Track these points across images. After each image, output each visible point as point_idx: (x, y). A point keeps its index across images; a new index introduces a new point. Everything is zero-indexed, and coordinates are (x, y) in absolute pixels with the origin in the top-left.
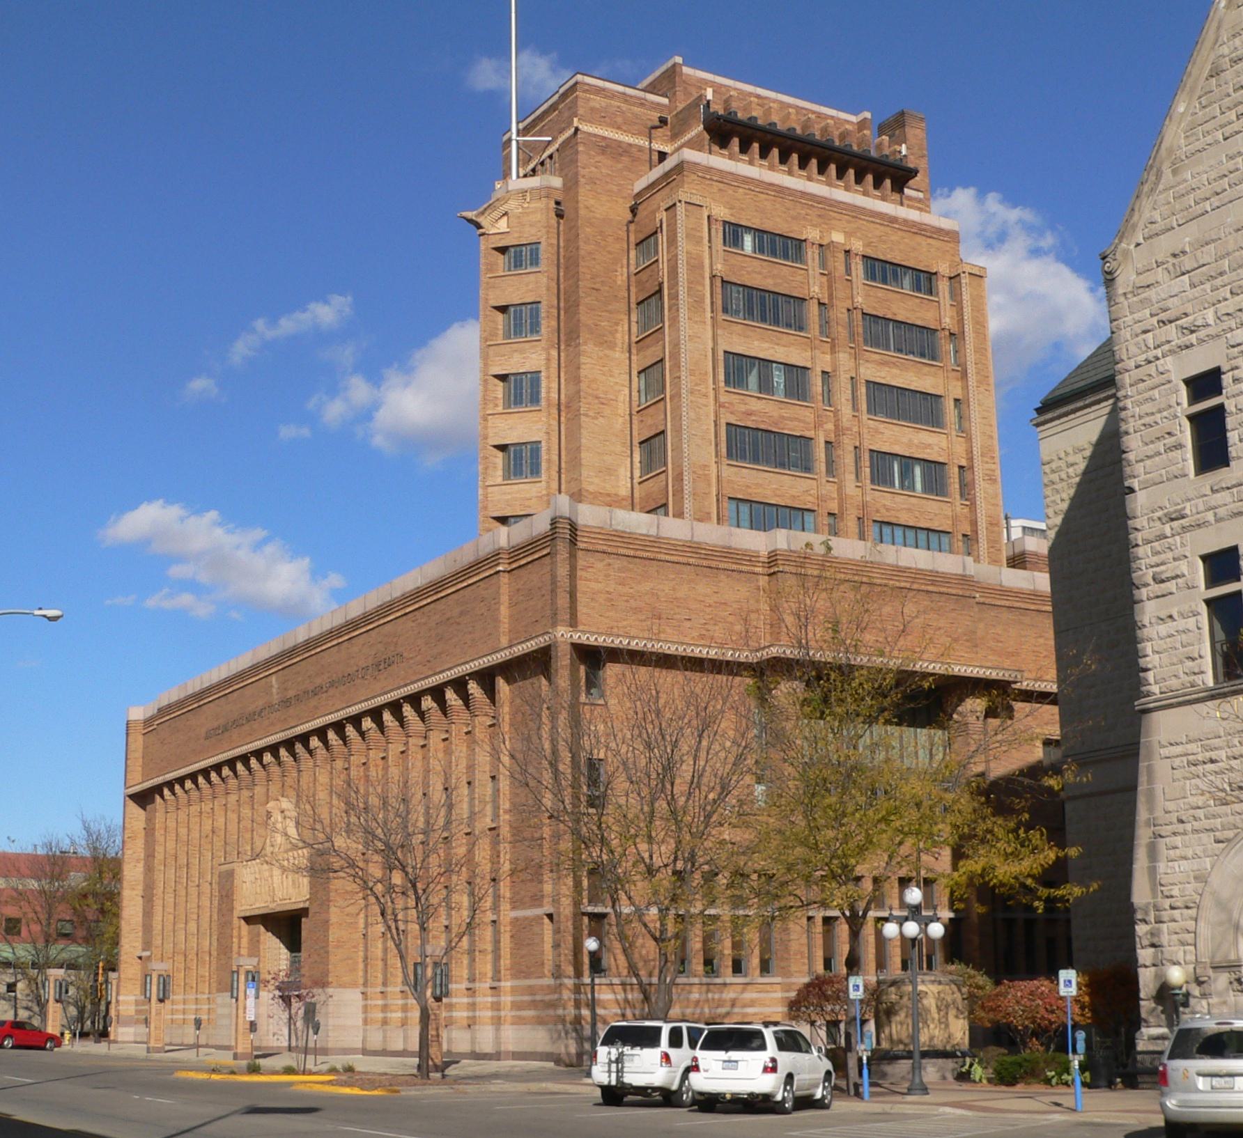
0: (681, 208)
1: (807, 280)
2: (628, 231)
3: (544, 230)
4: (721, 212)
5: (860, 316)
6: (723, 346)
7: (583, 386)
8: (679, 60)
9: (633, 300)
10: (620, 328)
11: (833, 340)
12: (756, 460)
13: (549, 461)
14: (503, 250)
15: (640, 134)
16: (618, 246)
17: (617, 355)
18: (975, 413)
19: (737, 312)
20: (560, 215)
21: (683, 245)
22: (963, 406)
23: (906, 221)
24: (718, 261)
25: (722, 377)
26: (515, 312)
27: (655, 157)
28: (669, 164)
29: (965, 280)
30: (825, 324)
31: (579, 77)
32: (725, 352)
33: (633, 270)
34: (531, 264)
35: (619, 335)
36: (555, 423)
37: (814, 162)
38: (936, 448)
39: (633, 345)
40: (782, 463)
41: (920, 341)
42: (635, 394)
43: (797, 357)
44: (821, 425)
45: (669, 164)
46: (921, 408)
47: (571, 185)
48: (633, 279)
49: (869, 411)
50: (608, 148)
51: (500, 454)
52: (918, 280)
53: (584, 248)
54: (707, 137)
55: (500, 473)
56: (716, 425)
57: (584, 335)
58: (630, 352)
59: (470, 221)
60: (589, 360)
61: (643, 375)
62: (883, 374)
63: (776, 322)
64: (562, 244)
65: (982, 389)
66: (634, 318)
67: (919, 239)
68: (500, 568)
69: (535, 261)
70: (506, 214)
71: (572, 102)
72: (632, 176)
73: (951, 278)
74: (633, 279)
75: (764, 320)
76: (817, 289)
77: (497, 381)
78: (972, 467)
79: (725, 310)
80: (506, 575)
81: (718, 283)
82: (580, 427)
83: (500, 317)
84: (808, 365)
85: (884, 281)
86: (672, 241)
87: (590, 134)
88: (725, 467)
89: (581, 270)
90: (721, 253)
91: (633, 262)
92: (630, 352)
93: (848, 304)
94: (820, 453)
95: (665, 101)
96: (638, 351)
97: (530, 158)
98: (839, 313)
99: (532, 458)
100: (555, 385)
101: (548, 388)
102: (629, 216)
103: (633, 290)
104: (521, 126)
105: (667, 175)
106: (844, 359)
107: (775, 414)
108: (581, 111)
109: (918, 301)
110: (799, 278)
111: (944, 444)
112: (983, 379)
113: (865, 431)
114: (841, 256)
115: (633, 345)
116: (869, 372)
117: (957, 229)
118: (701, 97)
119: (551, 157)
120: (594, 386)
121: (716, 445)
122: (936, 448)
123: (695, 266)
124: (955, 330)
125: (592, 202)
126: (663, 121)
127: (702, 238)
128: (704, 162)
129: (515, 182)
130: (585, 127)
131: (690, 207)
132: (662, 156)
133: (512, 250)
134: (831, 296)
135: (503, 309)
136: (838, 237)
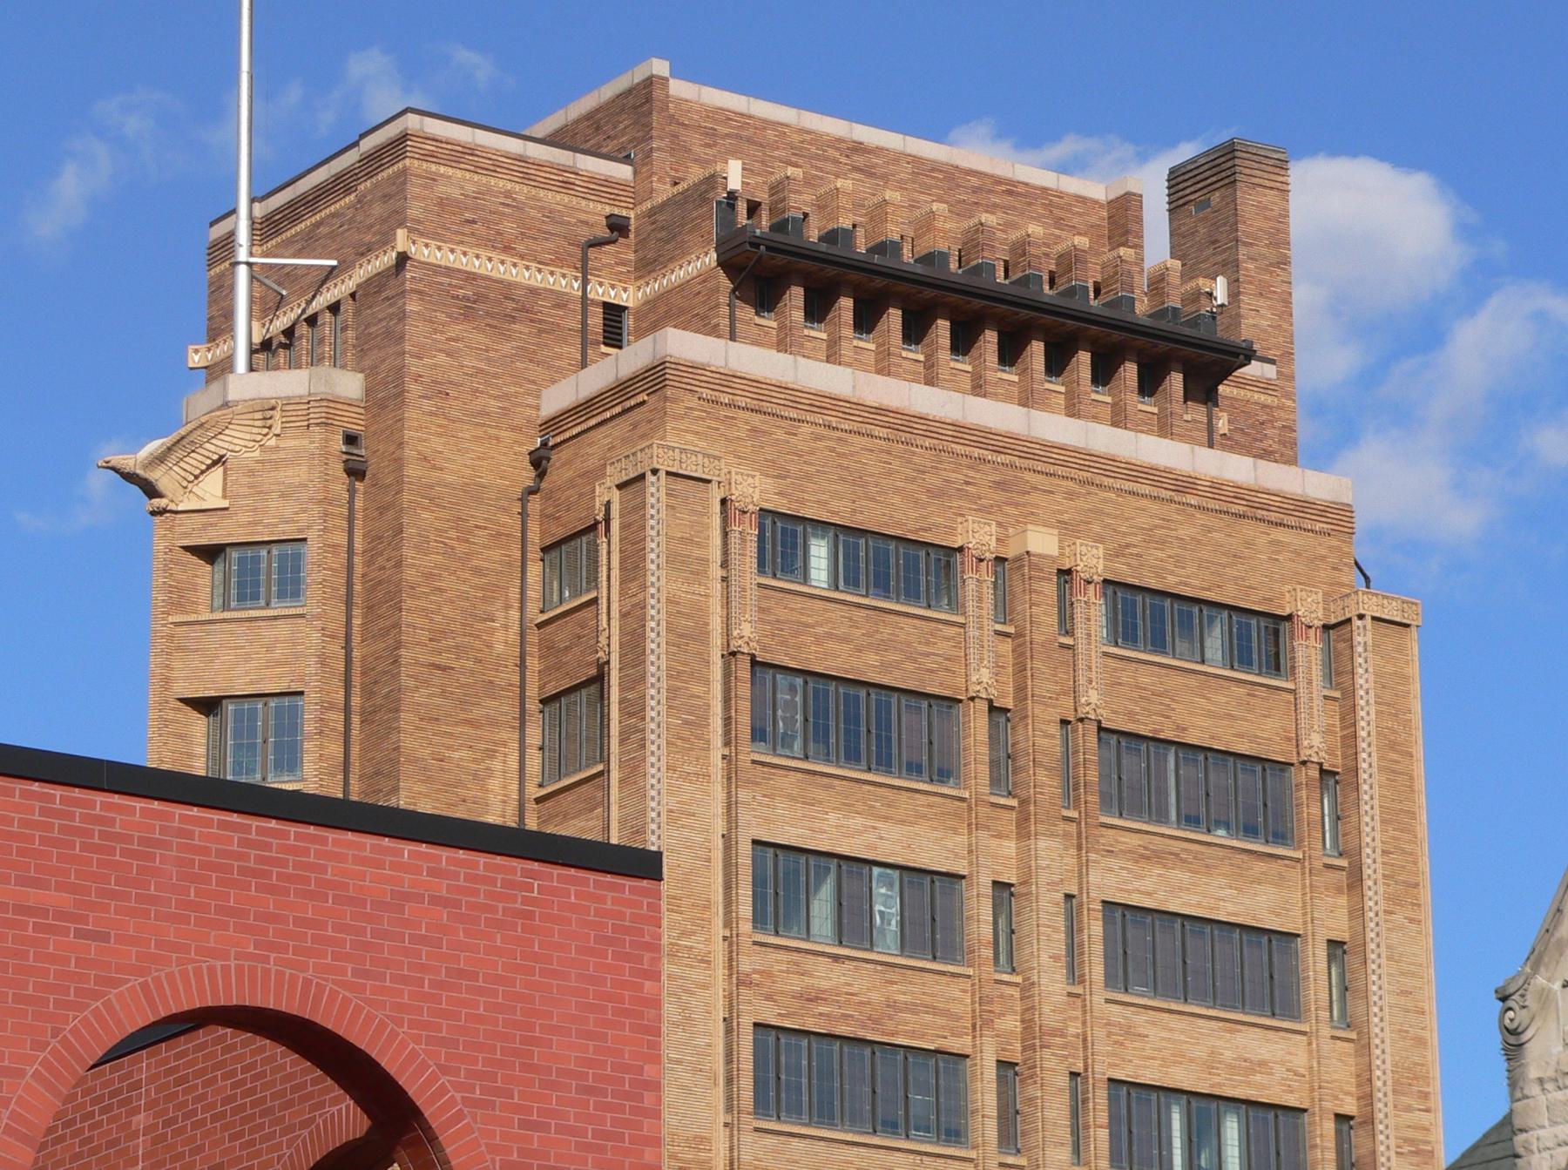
0: (656, 490)
1: (960, 651)
2: (524, 514)
3: (316, 510)
4: (754, 489)
5: (1092, 739)
6: (752, 827)
9: (533, 692)
10: (497, 765)
11: (1024, 802)
12: (824, 1114)
15: (559, 261)
16: (496, 554)
18: (1380, 980)
20: (355, 472)
21: (659, 578)
22: (1352, 961)
23: (1217, 486)
25: (745, 909)
27: (596, 320)
28: (633, 357)
29: (1363, 635)
30: (1005, 767)
33: (534, 615)
34: (282, 595)
35: (494, 784)
37: (990, 338)
38: (1280, 1072)
40: (890, 1121)
41: (1246, 796)
43: (933, 849)
45: (633, 357)
46: (1244, 968)
47: (385, 397)
48: (533, 637)
49: (1110, 981)
52: (1244, 636)
53: (415, 562)
54: (726, 283)
56: (729, 1031)
59: (130, 477)
62: (1148, 884)
63: (883, 762)
64: (359, 545)
65: (1398, 918)
66: (534, 736)
67: (1249, 529)
69: (291, 587)
70: (220, 461)
71: (391, 180)
72: (537, 372)
73: (1327, 628)
75: (852, 756)
76: (985, 675)
78: (1369, 1121)
79: (758, 735)
81: (743, 670)
83: (199, 725)
85: (1159, 645)
86: (633, 567)
87: (436, 269)
88: (747, 1138)
89: (406, 618)
90: (752, 594)
91: (534, 593)
93: (1066, 708)
94: (985, 1094)
95: (623, 172)
97: (281, 302)
98: (1040, 736)
102: (527, 475)
103: (533, 664)
104: (260, 210)
105: (623, 389)
106: (1052, 855)
107: (875, 997)
110: (943, 647)
111: (1300, 1060)
112: (1404, 893)
113: (1100, 1033)
114: (1049, 589)
116: (1112, 880)
117: (1347, 499)
118: (712, 181)
119: (334, 308)
121: (729, 1081)
122: (1280, 1072)
123: (688, 635)
124: (1334, 762)
125: (437, 443)
126: (618, 227)
127: (704, 561)
128: (718, 362)
129: (244, 384)
130: (424, 252)
131: (680, 485)
133: (234, 554)
134: (1020, 691)
136: (1042, 542)
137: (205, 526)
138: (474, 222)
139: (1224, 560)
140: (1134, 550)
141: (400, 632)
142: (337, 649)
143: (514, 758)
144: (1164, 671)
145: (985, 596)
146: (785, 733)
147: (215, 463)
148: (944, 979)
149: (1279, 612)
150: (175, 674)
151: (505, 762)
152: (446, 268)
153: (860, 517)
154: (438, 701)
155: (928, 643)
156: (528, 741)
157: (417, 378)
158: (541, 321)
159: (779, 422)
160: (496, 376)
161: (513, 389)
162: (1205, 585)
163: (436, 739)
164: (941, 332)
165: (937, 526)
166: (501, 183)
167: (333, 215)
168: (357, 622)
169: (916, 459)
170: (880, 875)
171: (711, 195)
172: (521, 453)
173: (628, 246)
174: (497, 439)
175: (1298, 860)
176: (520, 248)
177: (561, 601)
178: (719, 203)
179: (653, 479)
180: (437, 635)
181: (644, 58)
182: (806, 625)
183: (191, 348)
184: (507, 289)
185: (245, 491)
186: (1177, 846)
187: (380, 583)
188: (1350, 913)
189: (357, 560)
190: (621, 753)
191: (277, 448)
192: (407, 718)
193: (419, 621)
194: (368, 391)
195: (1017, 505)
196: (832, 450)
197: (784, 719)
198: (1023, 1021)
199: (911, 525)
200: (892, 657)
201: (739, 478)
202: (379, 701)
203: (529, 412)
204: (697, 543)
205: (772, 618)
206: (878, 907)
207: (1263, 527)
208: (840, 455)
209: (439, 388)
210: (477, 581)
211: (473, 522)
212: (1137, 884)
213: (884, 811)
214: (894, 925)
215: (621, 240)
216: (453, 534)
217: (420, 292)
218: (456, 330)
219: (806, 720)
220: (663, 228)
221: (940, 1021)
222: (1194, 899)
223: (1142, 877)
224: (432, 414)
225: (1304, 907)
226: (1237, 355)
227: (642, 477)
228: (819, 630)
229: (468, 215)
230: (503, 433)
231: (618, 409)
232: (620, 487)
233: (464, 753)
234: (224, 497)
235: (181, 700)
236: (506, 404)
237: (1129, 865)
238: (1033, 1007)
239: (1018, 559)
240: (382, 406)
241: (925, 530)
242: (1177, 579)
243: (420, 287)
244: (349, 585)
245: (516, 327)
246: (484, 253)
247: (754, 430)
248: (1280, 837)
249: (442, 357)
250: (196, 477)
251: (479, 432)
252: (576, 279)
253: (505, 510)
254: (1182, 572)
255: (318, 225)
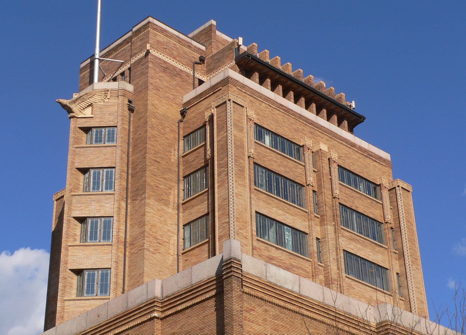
0: (230, 106)
3: (120, 118)
7: (147, 228)
8: (214, 22)
11: (322, 216)
13: (116, 283)
14: (87, 130)
15: (187, 65)
16: (172, 135)
17: (170, 210)
19: (261, 186)
20: (131, 110)
24: (251, 148)
26: (94, 173)
27: (197, 82)
31: (150, 19)
32: (256, 212)
34: (109, 141)
35: (171, 197)
36: (122, 255)
39: (181, 205)
42: (181, 241)
44: (317, 275)
47: (142, 89)
48: (181, 160)
50: (167, 69)
51: (75, 277)
55: (75, 291)
57: (148, 191)
58: (178, 209)
60: (152, 210)
61: (187, 228)
62: (352, 247)
66: (181, 187)
68: (156, 314)
69: (111, 138)
70: (91, 105)
71: (144, 35)
77: (76, 222)
80: (159, 321)
82: (143, 258)
84: (307, 231)
87: (156, 58)
89: (148, 146)
91: (181, 148)
92: (178, 209)
95: (203, 48)
96: (184, 210)
99: (102, 280)
100: (123, 227)
101: (117, 228)
102: (180, 117)
108: (151, 41)
109: (370, 201)
110: (299, 171)
115: (181, 205)
119: (123, 74)
120: (154, 230)
125: (157, 102)
129: (98, 85)
131: (236, 106)
132: (201, 82)
133: (94, 130)
135: (84, 171)
137: (86, 122)
141: (146, 150)
142: (125, 156)
143: (176, 191)
144: (351, 191)
147: (89, 106)
148: (305, 261)
150: (76, 161)
153: (278, 131)
154: (156, 171)
156: (180, 187)
157: (152, 84)
159: (257, 101)
161: (176, 94)
167: (122, 50)
168: (131, 150)
170: (286, 229)
171: (233, 47)
175: (386, 249)
176: (178, 59)
179: (229, 102)
180: (156, 153)
181: (209, 20)
182: (266, 156)
183: (74, 94)
184: (175, 68)
185: (99, 113)
186: (359, 238)
187: (139, 138)
188: (400, 266)
189: (131, 134)
190: (218, 179)
191: (108, 102)
192: (148, 173)
193: (152, 148)
194: (135, 90)
195: (315, 139)
196: (270, 112)
198: (325, 277)
199: (290, 137)
200: (287, 170)
202: (138, 170)
203: (180, 101)
206: (286, 237)
207: (371, 161)
208: (272, 114)
211: (165, 125)
212: (349, 246)
213: (287, 211)
214: (291, 242)
216: (160, 127)
217: (152, 62)
218: (161, 74)
220: (216, 60)
221: (304, 273)
222: (363, 253)
223: (350, 244)
224: (155, 94)
225: (389, 261)
226: (361, 118)
227: (225, 102)
228: (269, 158)
229: (165, 47)
232: (216, 107)
233: (163, 187)
234: (92, 114)
235: (77, 168)
237: (347, 240)
238: (329, 272)
239: (317, 151)
240: (140, 92)
243: (152, 61)
244: (129, 139)
248: (381, 241)
249: (158, 80)
250: (84, 109)
251: (167, 102)
253: (174, 125)
255: (117, 54)
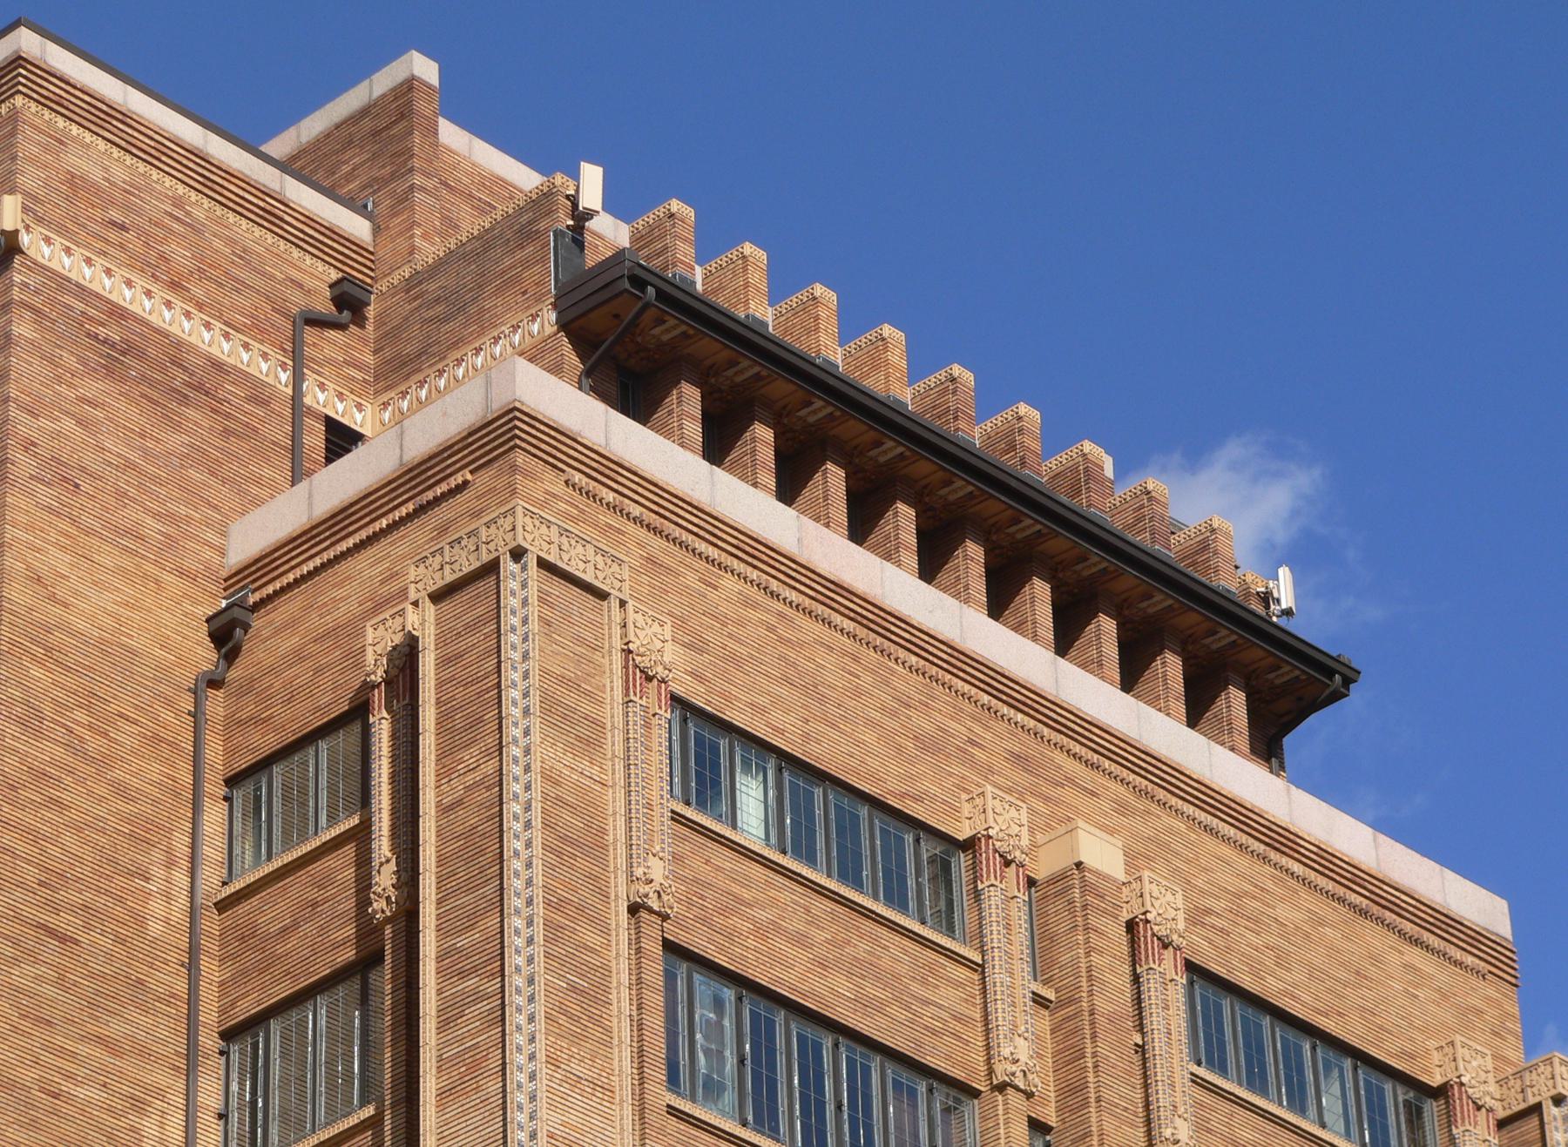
2: (197, 715)
8: (425, 69)
15: (255, 329)
16: (155, 771)
19: (712, 1090)
27: (315, 439)
66: (210, 1095)
74: (211, 923)
87: (62, 282)
95: (357, 227)
102: (205, 656)
103: (211, 970)
110: (948, 996)
125: (59, 560)
131: (558, 588)
132: (341, 439)
136: (1101, 853)
138: (123, 227)
139: (1342, 974)
140: (1219, 923)
143: (177, 1121)
145: (1015, 922)
146: (708, 1078)
149: (1425, 1079)
151: (162, 1125)
152: (78, 285)
154: (49, 991)
155: (924, 982)
157: (29, 446)
158: (228, 416)
160: (155, 480)
161: (183, 510)
162: (1319, 1005)
163: (46, 1057)
164: (902, 522)
165: (933, 798)
166: (168, 182)
169: (896, 682)
171: (542, 225)
172: (194, 616)
173: (364, 341)
174: (157, 582)
177: (269, 858)
178: (558, 234)
179: (513, 567)
182: (742, 902)
184: (177, 350)
190: (441, 1046)
195: (1047, 799)
196: (771, 629)
197: (707, 1052)
200: (872, 990)
201: (639, 617)
203: (208, 554)
204: (587, 693)
205: (687, 873)
207: (1393, 938)
208: (781, 639)
209: (63, 471)
210: (122, 806)
215: (353, 328)
218: (93, 387)
219: (742, 1061)
220: (437, 301)
224: (50, 509)
226: (1330, 673)
227: (492, 568)
229: (115, 215)
230: (167, 577)
231: (411, 507)
232: (437, 597)
236: (172, 531)
239: (1060, 878)
241: (916, 799)
242: (1281, 986)
243: (37, 301)
245: (191, 413)
246: (140, 282)
247: (650, 560)
249: (68, 424)
251: (126, 562)
252: (284, 366)
253: (169, 703)
254: (1288, 977)
